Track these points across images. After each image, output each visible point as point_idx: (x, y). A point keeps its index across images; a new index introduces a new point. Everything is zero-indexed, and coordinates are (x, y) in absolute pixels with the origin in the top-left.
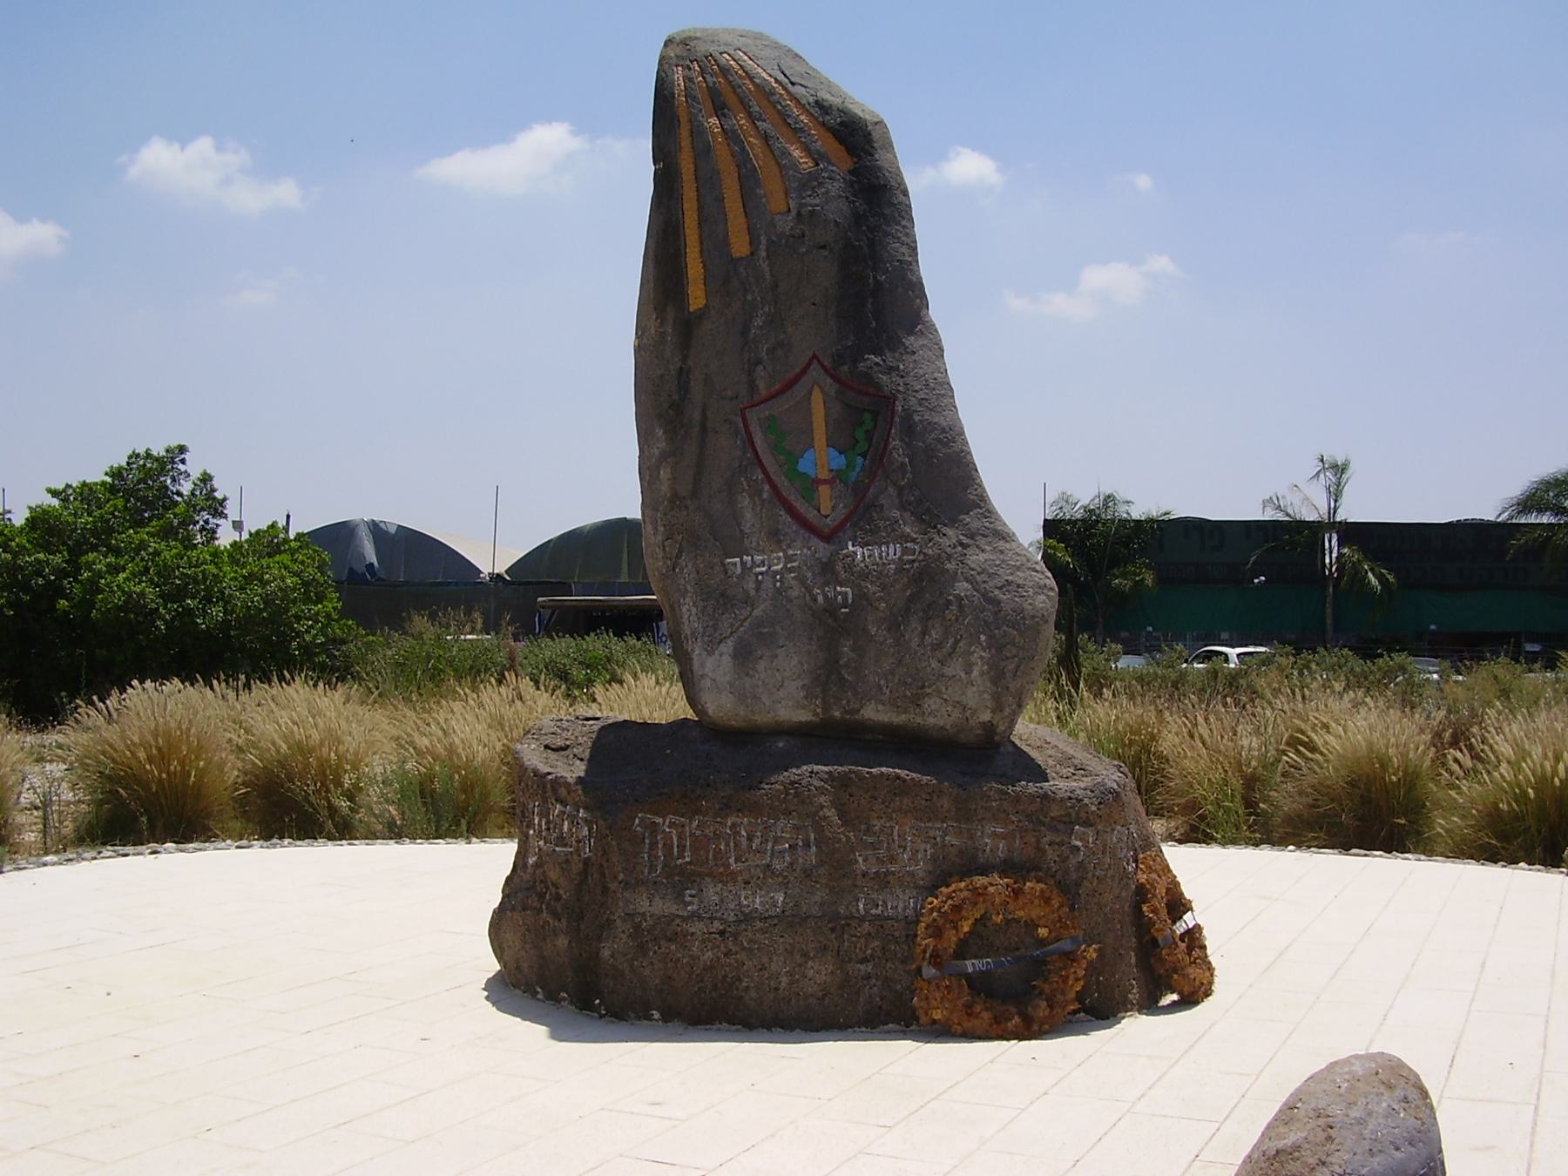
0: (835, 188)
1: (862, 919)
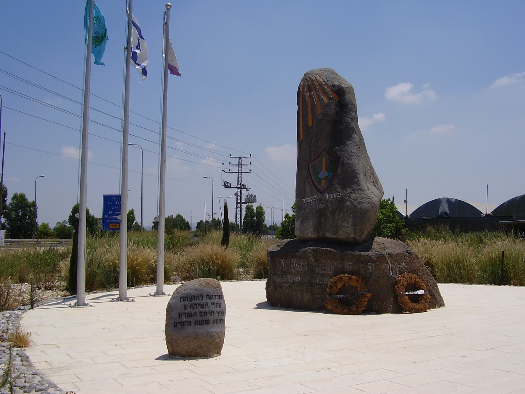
0: (333, 106)
1: (317, 284)
